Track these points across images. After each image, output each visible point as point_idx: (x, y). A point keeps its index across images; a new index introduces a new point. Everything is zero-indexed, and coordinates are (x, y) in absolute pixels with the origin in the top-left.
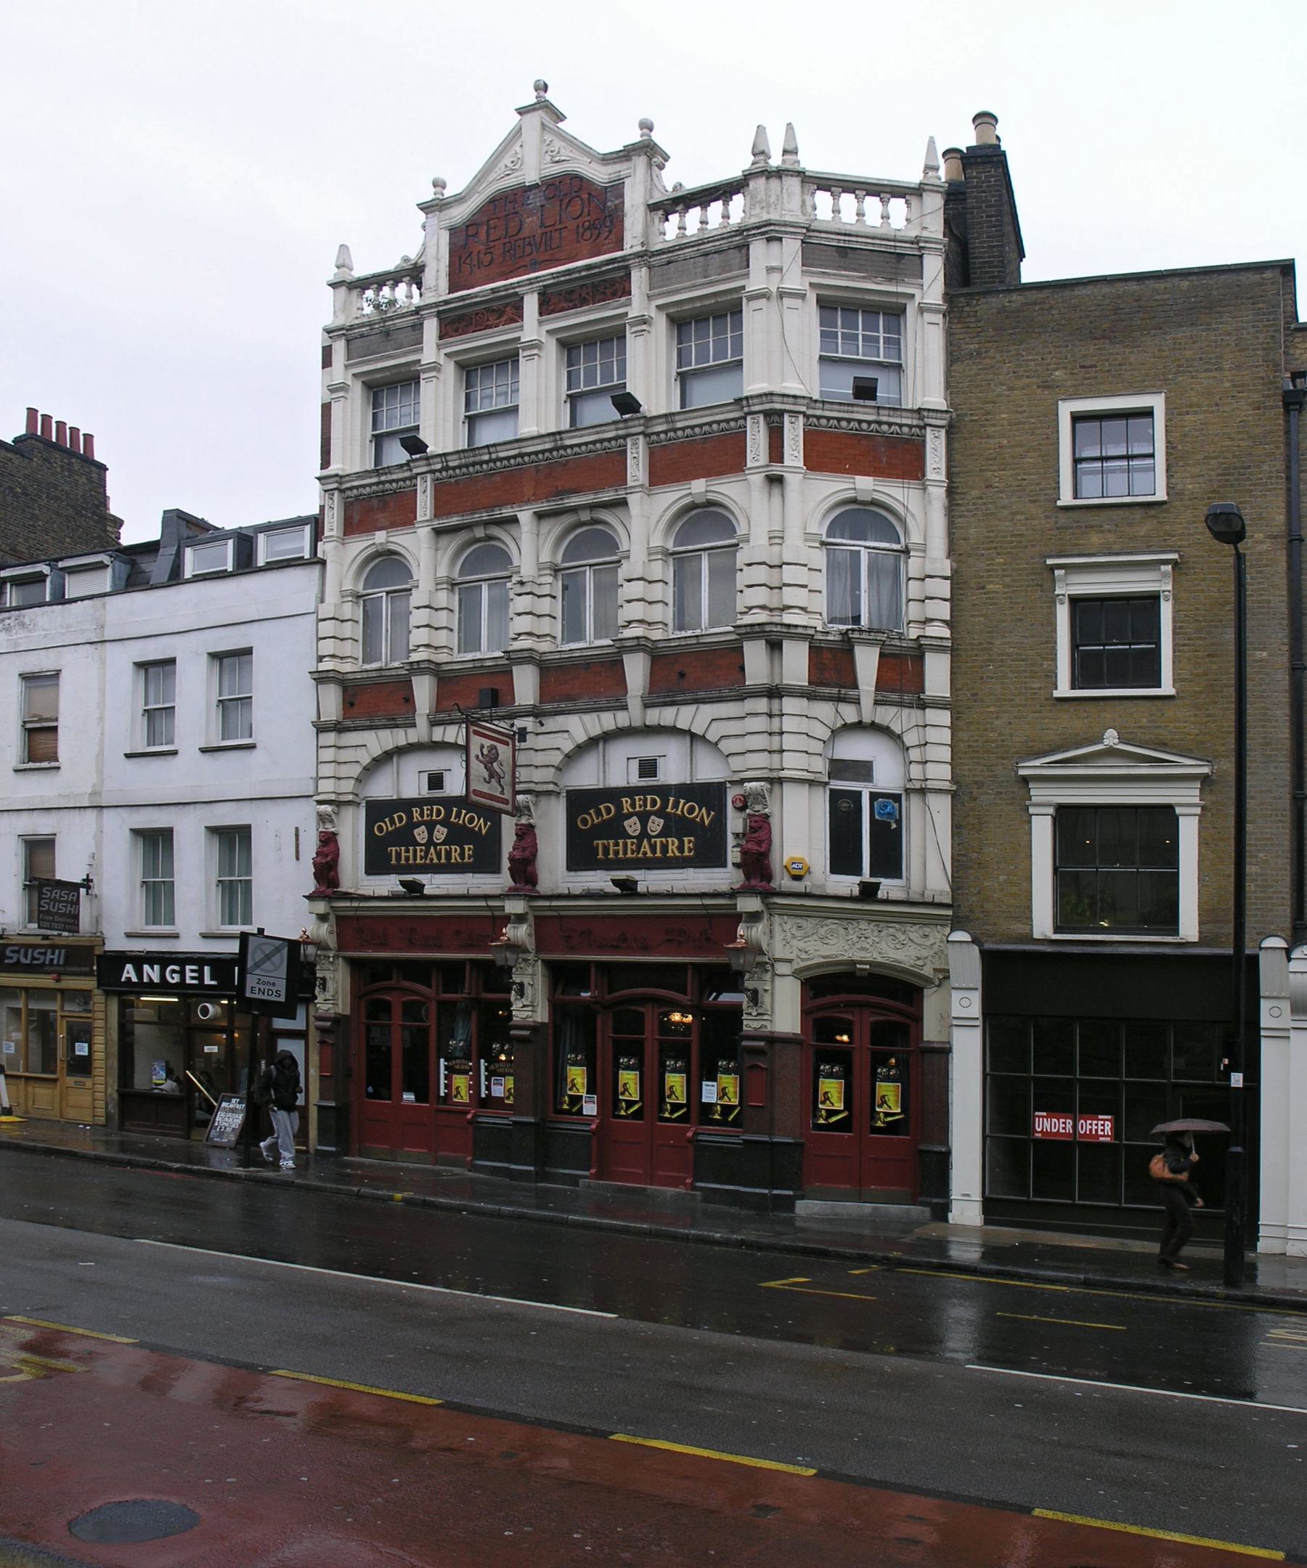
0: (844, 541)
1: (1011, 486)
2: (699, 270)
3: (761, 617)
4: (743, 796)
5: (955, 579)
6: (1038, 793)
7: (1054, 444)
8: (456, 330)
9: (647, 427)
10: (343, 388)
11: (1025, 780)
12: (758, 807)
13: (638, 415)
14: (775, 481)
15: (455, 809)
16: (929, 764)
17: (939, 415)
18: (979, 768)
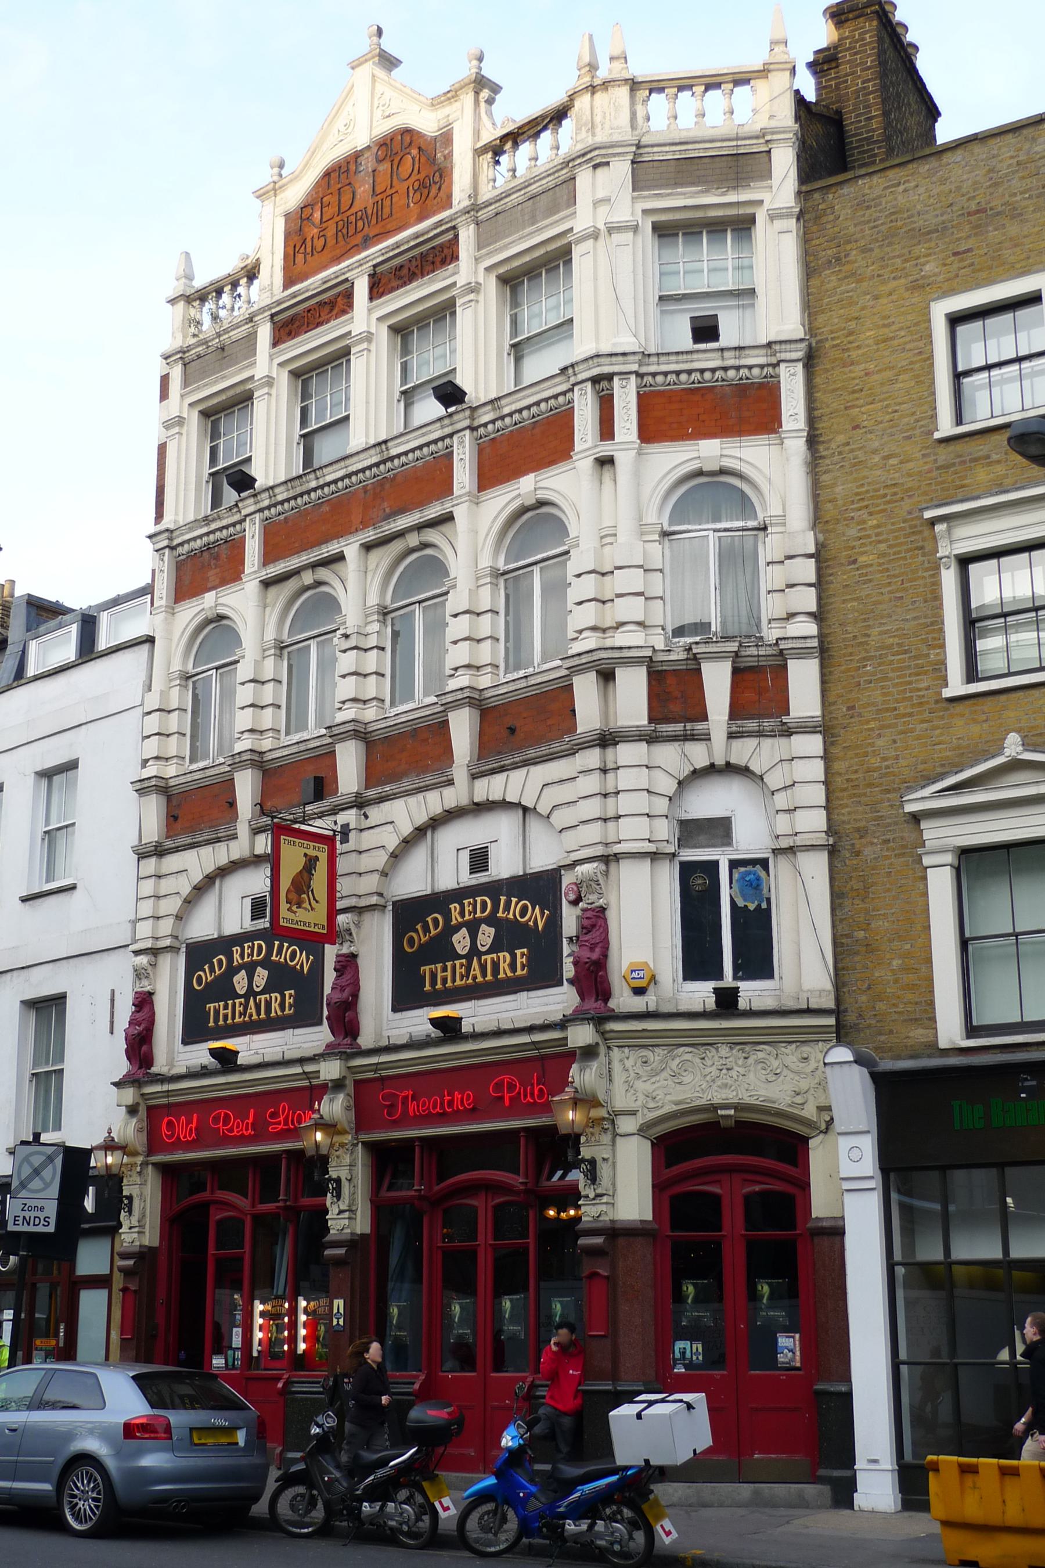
0: (690, 527)
1: (881, 422)
2: (526, 217)
3: (590, 642)
4: (575, 884)
5: (819, 556)
6: (933, 832)
7: (928, 358)
8: (289, 334)
9: (473, 420)
10: (180, 421)
11: (916, 818)
12: (592, 898)
13: (464, 406)
14: (605, 462)
15: (277, 943)
16: (798, 812)
17: (793, 346)
18: (860, 809)
